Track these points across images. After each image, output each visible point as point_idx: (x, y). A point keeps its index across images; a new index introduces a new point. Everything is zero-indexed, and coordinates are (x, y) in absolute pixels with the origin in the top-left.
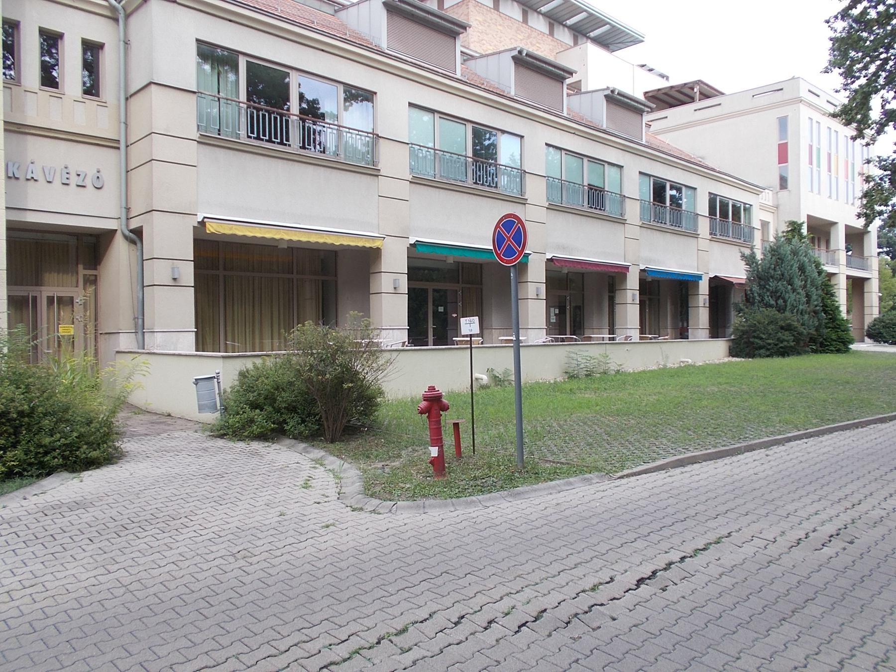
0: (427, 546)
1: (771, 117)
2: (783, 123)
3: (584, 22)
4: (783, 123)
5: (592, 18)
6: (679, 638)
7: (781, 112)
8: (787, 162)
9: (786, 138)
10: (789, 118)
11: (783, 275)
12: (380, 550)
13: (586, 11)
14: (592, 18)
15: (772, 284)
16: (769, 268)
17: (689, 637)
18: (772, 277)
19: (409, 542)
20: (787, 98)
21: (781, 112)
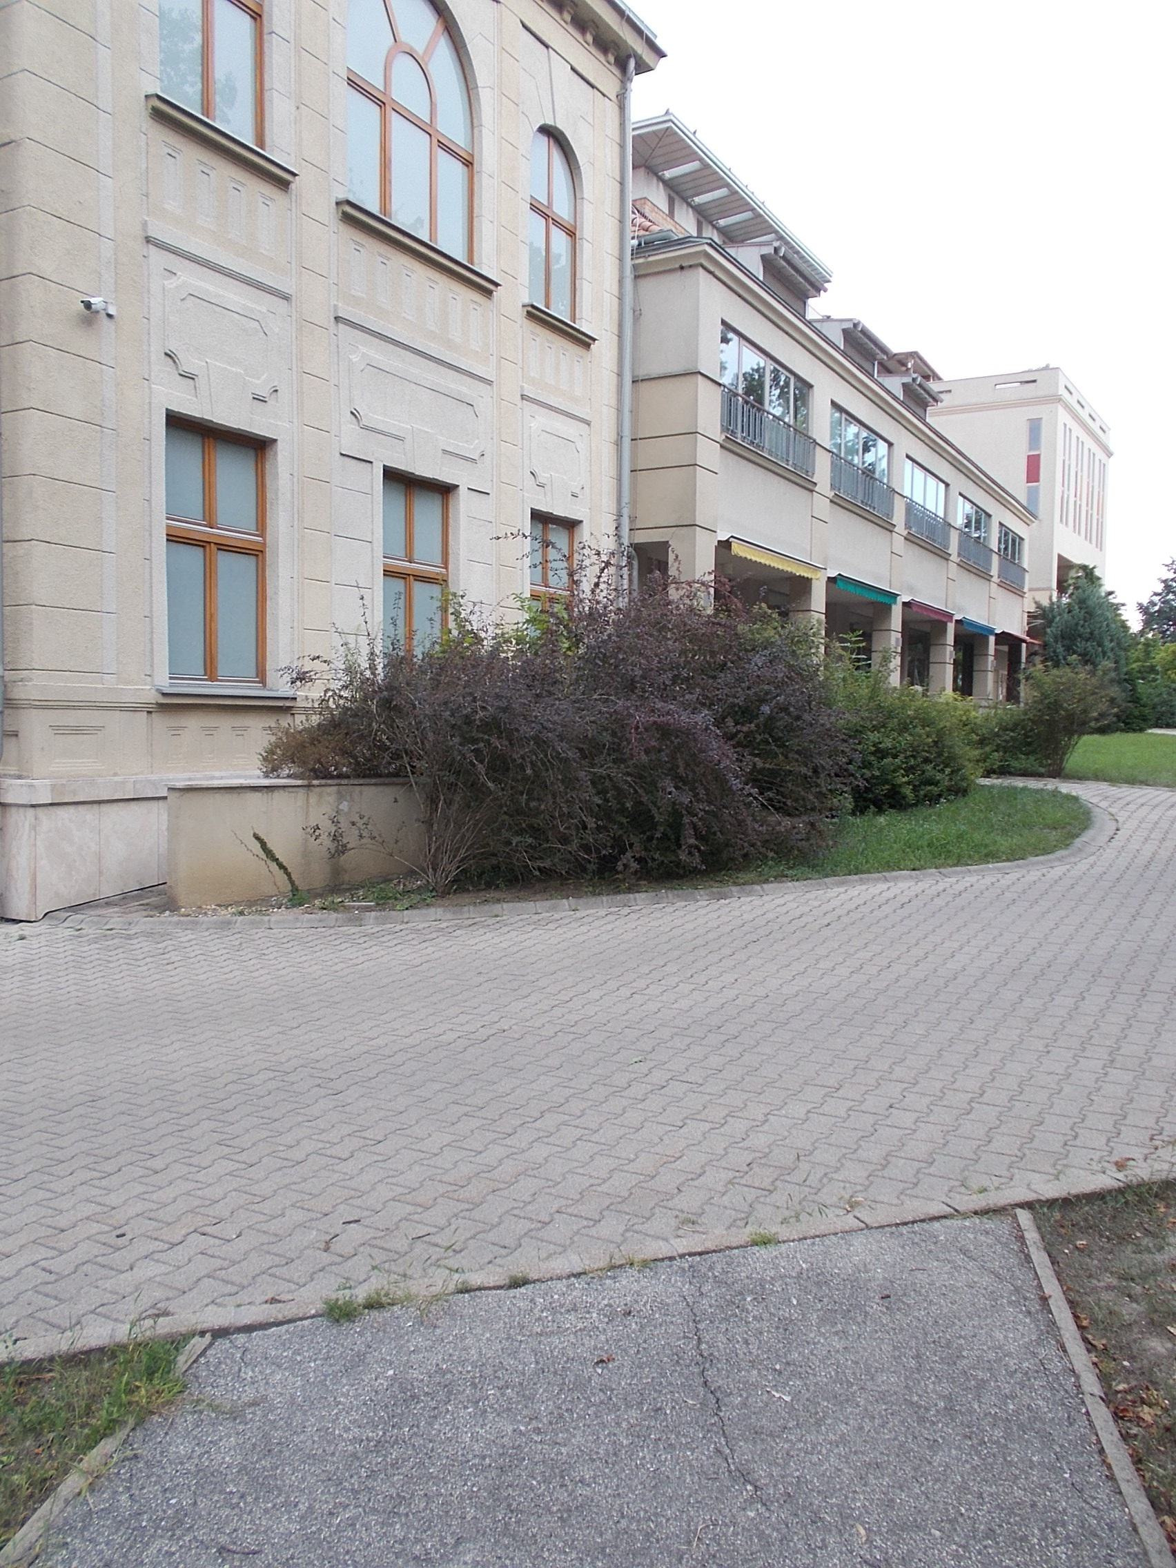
0: (225, 1162)
1: (1019, 419)
2: (1035, 428)
3: (683, 180)
4: (1035, 428)
5: (707, 172)
6: (902, 1185)
7: (1033, 412)
8: (1037, 481)
9: (1038, 448)
10: (1044, 422)
11: (1091, 633)
12: (49, 1221)
13: (701, 160)
14: (707, 172)
15: (1080, 645)
16: (1077, 624)
17: (884, 1162)
18: (1080, 636)
19: (241, 1245)
20: (956, 403)
21: (1033, 412)
